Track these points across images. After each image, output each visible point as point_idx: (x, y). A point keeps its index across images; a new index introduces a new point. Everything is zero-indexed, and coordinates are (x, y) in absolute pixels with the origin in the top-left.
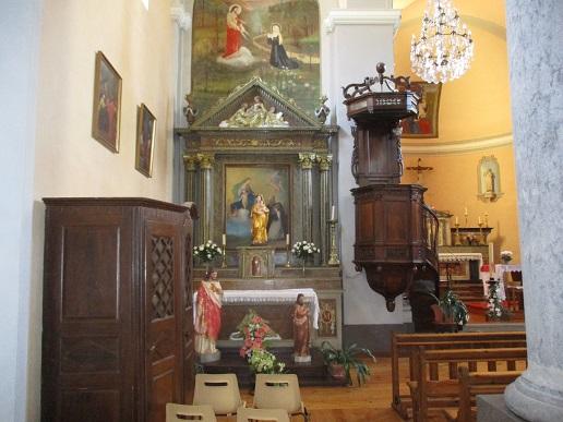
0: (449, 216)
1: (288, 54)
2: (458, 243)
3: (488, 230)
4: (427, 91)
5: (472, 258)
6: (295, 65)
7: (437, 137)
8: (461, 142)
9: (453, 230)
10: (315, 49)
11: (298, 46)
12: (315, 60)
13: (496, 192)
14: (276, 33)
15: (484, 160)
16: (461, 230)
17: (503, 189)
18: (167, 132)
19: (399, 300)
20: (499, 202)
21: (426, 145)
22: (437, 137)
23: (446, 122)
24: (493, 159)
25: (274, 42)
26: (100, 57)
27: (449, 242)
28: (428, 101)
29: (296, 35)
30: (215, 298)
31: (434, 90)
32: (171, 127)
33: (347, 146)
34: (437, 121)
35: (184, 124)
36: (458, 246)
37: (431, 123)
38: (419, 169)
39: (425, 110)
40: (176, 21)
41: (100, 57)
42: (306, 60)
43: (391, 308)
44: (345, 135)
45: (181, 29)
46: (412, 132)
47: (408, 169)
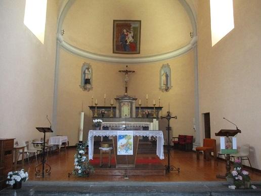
3: (160, 108)
4: (133, 26)
5: (144, 125)
7: (139, 53)
9: (137, 108)
13: (169, 86)
15: (163, 66)
16: (142, 108)
19: (26, 173)
20: (170, 91)
21: (133, 58)
22: (139, 53)
23: (144, 46)
26: (37, 128)
27: (134, 115)
28: (134, 32)
31: (137, 25)
34: (127, 21)
36: (139, 118)
37: (136, 45)
38: (127, 72)
39: (133, 37)
40: (119, 179)
41: (37, 128)
46: (125, 51)
47: (126, 92)
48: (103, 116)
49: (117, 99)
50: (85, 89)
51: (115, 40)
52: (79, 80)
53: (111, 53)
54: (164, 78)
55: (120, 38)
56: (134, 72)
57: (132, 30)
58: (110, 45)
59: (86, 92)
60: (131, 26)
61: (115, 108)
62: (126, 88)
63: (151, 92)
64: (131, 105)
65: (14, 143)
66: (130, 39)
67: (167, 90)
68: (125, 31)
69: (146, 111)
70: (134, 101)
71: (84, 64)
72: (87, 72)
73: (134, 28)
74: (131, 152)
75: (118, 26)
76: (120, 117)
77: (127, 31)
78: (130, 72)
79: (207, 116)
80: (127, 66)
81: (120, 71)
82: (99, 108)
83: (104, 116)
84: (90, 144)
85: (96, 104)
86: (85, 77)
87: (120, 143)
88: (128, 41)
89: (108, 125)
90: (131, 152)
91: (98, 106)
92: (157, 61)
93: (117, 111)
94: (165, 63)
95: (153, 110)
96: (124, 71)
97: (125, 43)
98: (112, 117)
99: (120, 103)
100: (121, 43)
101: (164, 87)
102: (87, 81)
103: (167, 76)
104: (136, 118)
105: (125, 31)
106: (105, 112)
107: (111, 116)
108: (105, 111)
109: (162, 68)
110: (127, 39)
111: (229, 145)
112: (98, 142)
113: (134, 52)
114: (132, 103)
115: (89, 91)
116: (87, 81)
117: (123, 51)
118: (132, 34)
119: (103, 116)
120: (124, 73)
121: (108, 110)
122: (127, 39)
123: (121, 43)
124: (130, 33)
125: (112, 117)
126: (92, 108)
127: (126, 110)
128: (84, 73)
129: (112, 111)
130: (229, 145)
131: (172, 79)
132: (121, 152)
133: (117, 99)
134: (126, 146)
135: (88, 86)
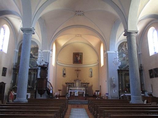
0: (80, 80)
1: (33, 56)
2: (82, 86)
3: (89, 83)
6: (34, 58)
7: (82, 64)
8: (72, 67)
9: (81, 83)
10: (37, 55)
11: (34, 55)
12: (37, 57)
14: (32, 52)
17: (93, 75)
18: (12, 69)
22: (82, 64)
23: (84, 61)
24: (92, 69)
25: (31, 54)
29: (35, 53)
30: (13, 94)
31: (81, 54)
32: (13, 67)
33: (39, 71)
35: (15, 67)
38: (78, 70)
39: (80, 58)
42: (36, 57)
43: (41, 96)
44: (39, 69)
45: (16, 52)
49: (75, 80)
50: (64, 77)
52: (62, 74)
54: (90, 73)
58: (72, 61)
61: (74, 83)
63: (86, 78)
65: (117, 87)
66: (79, 59)
67: (91, 77)
68: (77, 56)
69: (84, 84)
72: (64, 71)
74: (78, 95)
75: (75, 54)
76: (76, 86)
79: (101, 86)
84: (69, 93)
87: (75, 93)
90: (78, 95)
93: (75, 85)
94: (91, 67)
99: (75, 82)
101: (90, 76)
102: (64, 74)
103: (91, 72)
105: (77, 56)
109: (90, 69)
111: (97, 94)
112: (71, 93)
114: (79, 82)
126: (66, 83)
127: (77, 84)
128: (64, 71)
130: (97, 94)
132: (75, 95)
133: (75, 80)
134: (76, 94)
135: (65, 76)
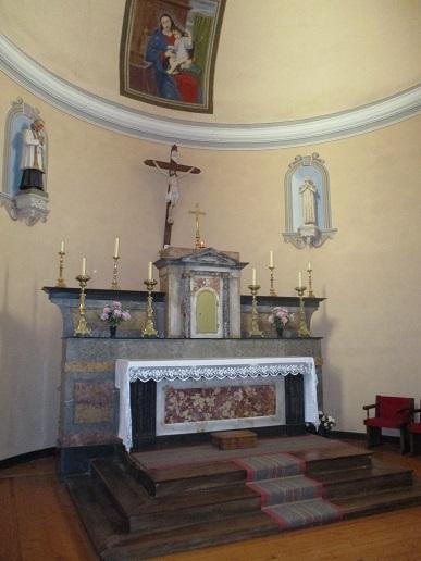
7: (210, 111)
9: (245, 300)
15: (298, 162)
20: (329, 246)
22: (210, 111)
23: (227, 86)
38: (172, 167)
39: (191, 53)
46: (163, 95)
48: (113, 331)
50: (18, 212)
51: (128, 49)
53: (113, 91)
55: (144, 47)
56: (197, 171)
57: (188, 23)
59: (22, 224)
60: (190, 8)
62: (168, 227)
64: (227, 288)
66: (179, 57)
67: (316, 240)
70: (234, 273)
71: (17, 107)
72: (29, 137)
73: (199, 19)
77: (173, 27)
78: (186, 169)
80: (174, 148)
81: (150, 163)
82: (94, 294)
83: (117, 335)
85: (79, 279)
86: (19, 157)
88: (173, 64)
89: (209, 372)
91: (89, 286)
92: (273, 143)
95: (294, 309)
96: (163, 165)
97: (160, 68)
98: (153, 338)
100: (149, 64)
104: (244, 336)
106: (126, 315)
107: (150, 329)
108: (123, 309)
110: (168, 54)
113: (195, 106)
115: (32, 221)
116: (30, 180)
117: (154, 94)
118: (188, 41)
119: (113, 331)
120: (165, 172)
121: (132, 304)
122: (168, 54)
123: (149, 64)
124: (183, 34)
125: (153, 338)
128: (18, 143)
129: (151, 310)
131: (333, 207)
135: (33, 198)
